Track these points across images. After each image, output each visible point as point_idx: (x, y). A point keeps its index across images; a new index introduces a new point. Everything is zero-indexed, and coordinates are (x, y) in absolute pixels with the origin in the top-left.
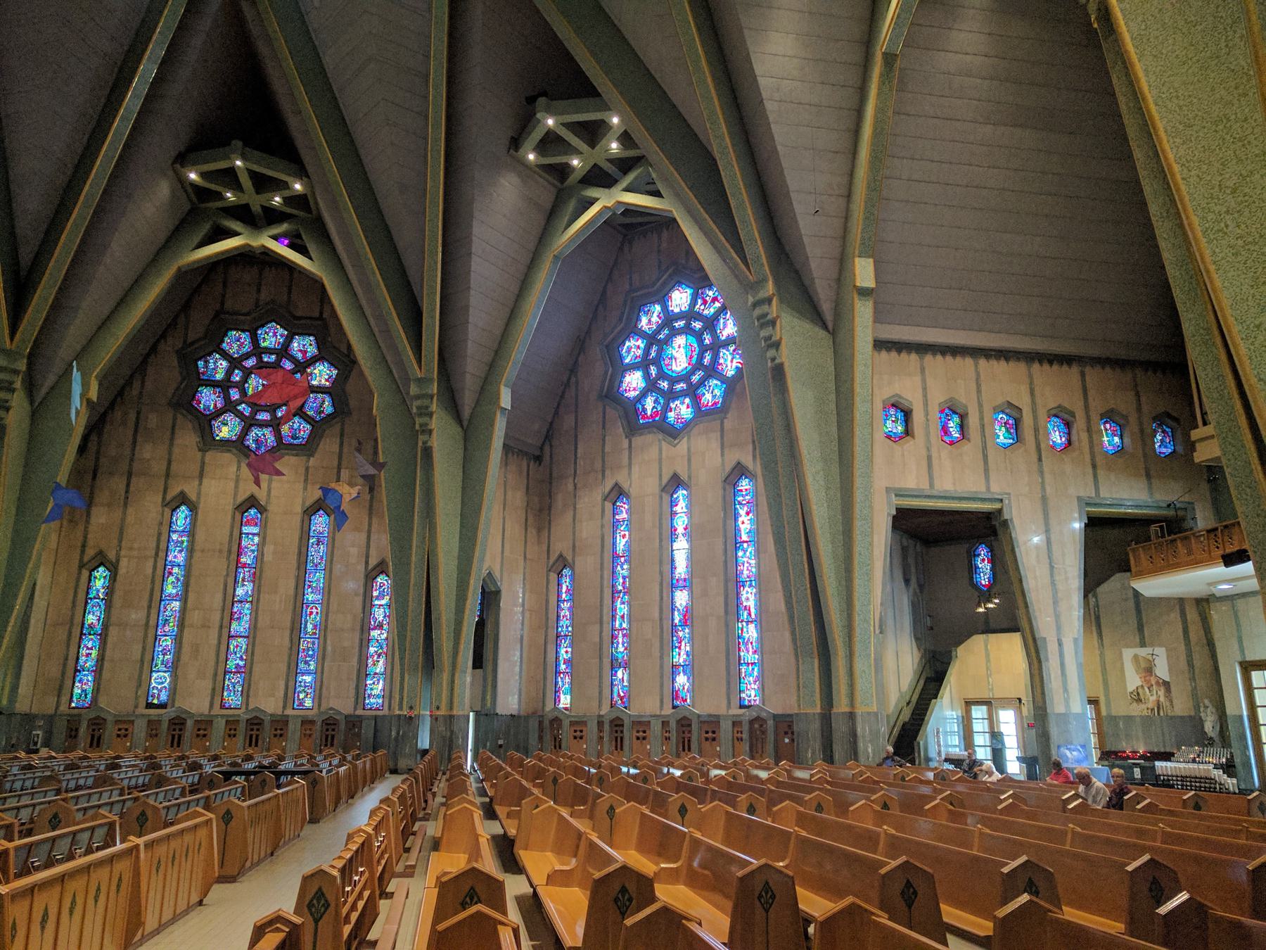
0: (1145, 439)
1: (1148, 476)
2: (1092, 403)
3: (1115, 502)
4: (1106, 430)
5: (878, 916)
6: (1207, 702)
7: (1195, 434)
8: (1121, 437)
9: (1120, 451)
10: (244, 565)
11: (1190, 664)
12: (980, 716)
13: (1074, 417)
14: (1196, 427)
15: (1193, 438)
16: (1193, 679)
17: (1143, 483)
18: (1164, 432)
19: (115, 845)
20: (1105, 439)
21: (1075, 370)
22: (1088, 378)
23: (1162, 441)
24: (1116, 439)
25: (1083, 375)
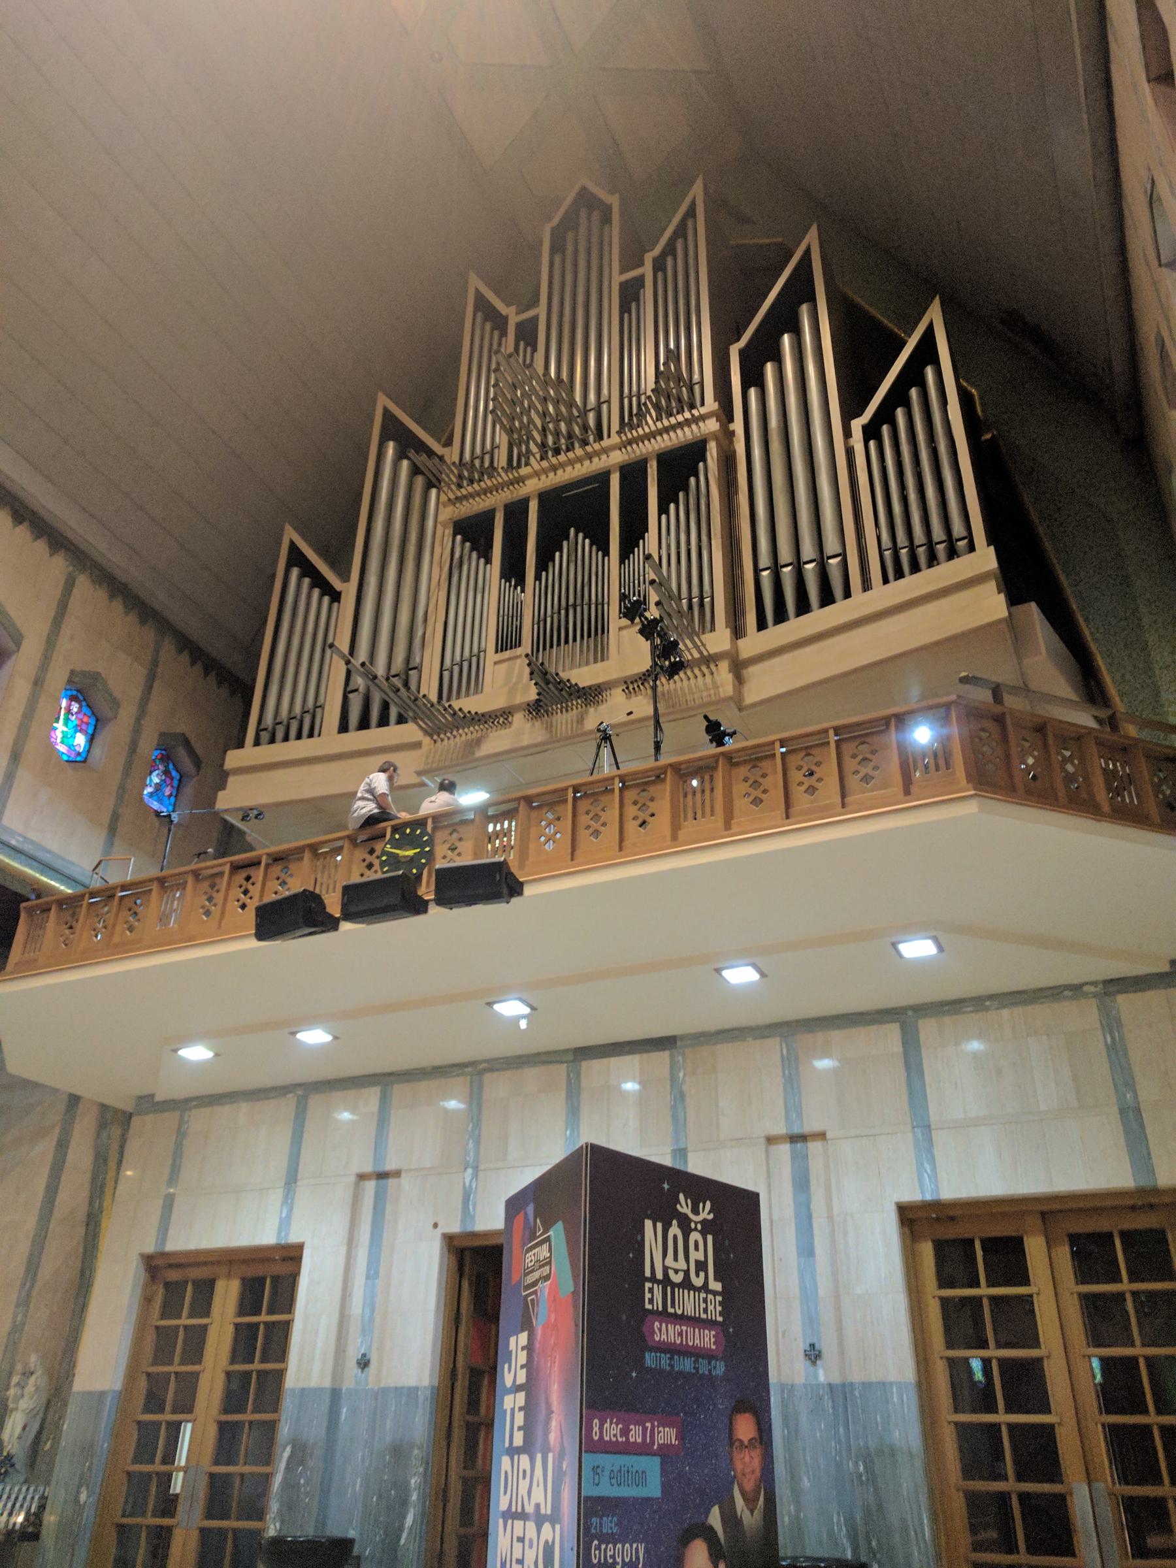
0: (132, 771)
1: (112, 830)
2: (64, 644)
3: (27, 847)
4: (69, 711)
5: (13, 1429)
6: (33, 1359)
7: (234, 759)
8: (91, 740)
9: (80, 762)
10: (517, 1388)
11: (32, 1266)
12: (539, 1497)
13: (18, 644)
14: (240, 745)
15: (228, 765)
16: (24, 1303)
17: (97, 840)
18: (166, 772)
19: (252, 1362)
20: (60, 726)
21: (59, 565)
22: (76, 592)
23: (158, 788)
24: (80, 740)
25: (70, 585)
